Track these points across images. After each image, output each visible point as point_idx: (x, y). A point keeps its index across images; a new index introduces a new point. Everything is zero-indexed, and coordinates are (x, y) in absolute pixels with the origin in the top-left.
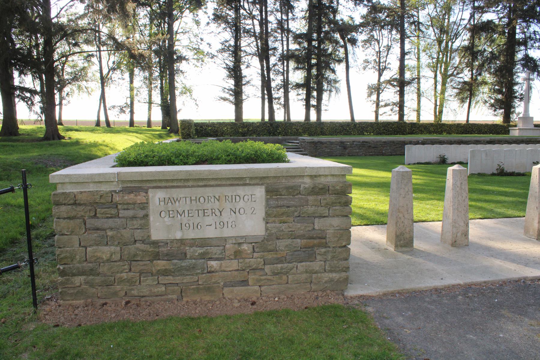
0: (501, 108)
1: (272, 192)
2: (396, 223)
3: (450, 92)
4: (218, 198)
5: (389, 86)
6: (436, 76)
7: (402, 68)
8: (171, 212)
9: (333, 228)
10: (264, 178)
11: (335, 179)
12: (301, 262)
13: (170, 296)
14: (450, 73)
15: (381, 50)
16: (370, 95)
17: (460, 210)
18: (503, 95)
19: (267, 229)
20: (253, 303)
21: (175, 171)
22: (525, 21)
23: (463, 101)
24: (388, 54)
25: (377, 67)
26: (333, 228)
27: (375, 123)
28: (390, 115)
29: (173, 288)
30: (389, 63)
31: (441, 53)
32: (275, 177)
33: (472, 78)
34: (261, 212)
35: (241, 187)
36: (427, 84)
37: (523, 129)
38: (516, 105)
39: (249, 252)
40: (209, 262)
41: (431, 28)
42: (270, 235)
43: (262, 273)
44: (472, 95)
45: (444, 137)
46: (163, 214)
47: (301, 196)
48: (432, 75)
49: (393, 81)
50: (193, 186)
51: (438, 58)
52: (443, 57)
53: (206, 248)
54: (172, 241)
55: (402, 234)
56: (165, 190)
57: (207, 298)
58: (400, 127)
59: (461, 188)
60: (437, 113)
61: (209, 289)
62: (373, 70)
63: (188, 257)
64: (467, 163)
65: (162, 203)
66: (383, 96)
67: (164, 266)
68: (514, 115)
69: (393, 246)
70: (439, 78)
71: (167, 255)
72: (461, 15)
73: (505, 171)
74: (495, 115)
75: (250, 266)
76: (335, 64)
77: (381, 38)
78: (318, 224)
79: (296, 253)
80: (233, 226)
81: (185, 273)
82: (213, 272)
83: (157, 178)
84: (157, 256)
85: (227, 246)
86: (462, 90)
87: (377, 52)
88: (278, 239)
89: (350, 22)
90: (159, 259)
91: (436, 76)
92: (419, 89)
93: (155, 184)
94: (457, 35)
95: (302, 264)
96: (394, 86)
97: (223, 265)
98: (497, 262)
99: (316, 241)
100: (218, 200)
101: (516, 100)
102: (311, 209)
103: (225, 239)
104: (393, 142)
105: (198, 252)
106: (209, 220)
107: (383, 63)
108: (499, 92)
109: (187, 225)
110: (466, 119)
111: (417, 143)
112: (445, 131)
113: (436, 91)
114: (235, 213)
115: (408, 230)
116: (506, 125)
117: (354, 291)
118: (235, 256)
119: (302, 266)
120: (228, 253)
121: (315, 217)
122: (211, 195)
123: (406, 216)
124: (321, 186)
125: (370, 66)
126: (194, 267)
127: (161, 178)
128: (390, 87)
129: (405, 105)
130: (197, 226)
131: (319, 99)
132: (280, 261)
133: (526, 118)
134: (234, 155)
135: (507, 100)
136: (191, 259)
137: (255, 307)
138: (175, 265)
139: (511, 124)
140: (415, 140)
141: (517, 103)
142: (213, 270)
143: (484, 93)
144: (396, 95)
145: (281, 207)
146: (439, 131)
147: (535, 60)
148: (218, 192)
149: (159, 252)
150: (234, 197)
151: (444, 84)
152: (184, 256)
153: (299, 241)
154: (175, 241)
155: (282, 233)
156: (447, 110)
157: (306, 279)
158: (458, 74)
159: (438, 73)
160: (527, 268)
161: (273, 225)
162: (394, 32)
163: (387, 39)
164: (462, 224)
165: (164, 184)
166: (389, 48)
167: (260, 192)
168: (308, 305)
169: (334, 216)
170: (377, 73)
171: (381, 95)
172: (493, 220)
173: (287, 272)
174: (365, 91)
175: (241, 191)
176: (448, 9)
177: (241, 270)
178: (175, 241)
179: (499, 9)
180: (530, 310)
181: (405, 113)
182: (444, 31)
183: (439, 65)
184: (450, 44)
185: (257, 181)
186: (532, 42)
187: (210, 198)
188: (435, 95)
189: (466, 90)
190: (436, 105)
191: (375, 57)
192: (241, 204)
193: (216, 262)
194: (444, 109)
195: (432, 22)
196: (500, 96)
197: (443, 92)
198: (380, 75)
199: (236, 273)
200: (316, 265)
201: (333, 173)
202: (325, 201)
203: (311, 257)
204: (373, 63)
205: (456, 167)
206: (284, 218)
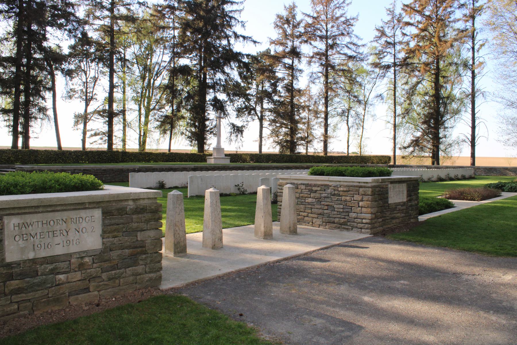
1: (106, 213)
2: (174, 235)
3: (153, 124)
4: (65, 220)
5: (96, 116)
6: (140, 109)
7: (110, 100)
8: (25, 236)
9: (150, 239)
10: (100, 202)
11: (150, 201)
12: (129, 267)
13: (21, 313)
14: (151, 107)
15: (88, 81)
16: (77, 123)
17: (216, 221)
19: (103, 243)
20: (98, 305)
21: (29, 200)
22: (212, 69)
23: (164, 132)
24: (94, 85)
25: (84, 97)
26: (150, 239)
29: (25, 304)
30: (95, 94)
32: (108, 201)
33: (172, 113)
34: (99, 230)
35: (84, 211)
37: (217, 158)
38: (208, 137)
39: (90, 263)
40: (57, 276)
41: (136, 65)
42: (105, 248)
43: (100, 280)
44: (172, 127)
45: (177, 164)
46: (17, 238)
47: (127, 216)
48: (137, 107)
50: (42, 212)
51: (142, 92)
53: (55, 264)
54: (25, 261)
55: (178, 243)
56: (20, 216)
57: (56, 308)
58: (110, 155)
59: (216, 205)
61: (57, 300)
62: (79, 99)
63: (39, 274)
64: (187, 187)
65: (17, 228)
66: (90, 125)
67: (17, 285)
69: (173, 253)
70: (143, 111)
71: (20, 274)
75: (91, 275)
76: (45, 92)
77: (88, 69)
78: (140, 236)
79: (125, 260)
80: (78, 243)
81: (37, 288)
82: (62, 284)
83: (12, 206)
84: (11, 277)
85: (73, 260)
86: (163, 123)
87: (84, 83)
88: (111, 250)
89: (58, 51)
90: (13, 280)
91: (140, 109)
92: (124, 120)
93: (8, 212)
94: (158, 74)
95: (129, 269)
96: (103, 116)
97: (69, 277)
98: (248, 256)
99: (139, 250)
100: (65, 222)
101: (208, 133)
102: (135, 225)
103: (70, 255)
104: (112, 170)
105: (49, 268)
106: (58, 240)
107: (89, 93)
109: (39, 246)
110: (168, 148)
111: (139, 170)
114: (79, 232)
115: (182, 239)
117: (166, 286)
118: (79, 268)
119: (130, 270)
120: (73, 267)
121: (138, 231)
122: (60, 218)
123: (181, 229)
124: (141, 207)
125: (77, 96)
126: (45, 282)
127: (16, 206)
128: (100, 117)
129: (114, 134)
130: (48, 246)
131: (26, 127)
132: (113, 268)
133: (218, 149)
134: (64, 184)
136: (42, 275)
137: (100, 307)
138: (28, 282)
140: (132, 168)
141: (209, 136)
142: (61, 282)
144: (105, 125)
145: (113, 225)
146: (145, 159)
148: (65, 215)
149: (12, 273)
150: (78, 219)
151: (147, 116)
152: (36, 274)
153: (127, 250)
154: (27, 262)
155: (114, 246)
157: (133, 280)
158: (160, 109)
159: (142, 106)
160: (267, 257)
161: (108, 240)
162: (101, 65)
163: (94, 71)
164: (218, 232)
165: (16, 211)
166: (95, 79)
167: (97, 214)
168: (139, 300)
169: (150, 230)
170: (83, 103)
171: (88, 124)
172: (229, 229)
173: (119, 277)
174: (72, 121)
175: (83, 213)
177: (83, 280)
178: (27, 262)
179: (191, 56)
180: (281, 278)
181: (114, 142)
184: (152, 81)
185: (95, 205)
186: (218, 87)
187: (58, 221)
188: (140, 125)
189: (167, 123)
190: (140, 135)
191: (82, 88)
192: (84, 224)
193: (64, 275)
194: (148, 139)
195: (137, 60)
196: (193, 130)
197: (146, 124)
198: (87, 105)
199: (80, 282)
200: (140, 269)
201: (149, 197)
202: (144, 218)
203: (135, 263)
204: (80, 92)
205: (174, 192)
206: (115, 234)
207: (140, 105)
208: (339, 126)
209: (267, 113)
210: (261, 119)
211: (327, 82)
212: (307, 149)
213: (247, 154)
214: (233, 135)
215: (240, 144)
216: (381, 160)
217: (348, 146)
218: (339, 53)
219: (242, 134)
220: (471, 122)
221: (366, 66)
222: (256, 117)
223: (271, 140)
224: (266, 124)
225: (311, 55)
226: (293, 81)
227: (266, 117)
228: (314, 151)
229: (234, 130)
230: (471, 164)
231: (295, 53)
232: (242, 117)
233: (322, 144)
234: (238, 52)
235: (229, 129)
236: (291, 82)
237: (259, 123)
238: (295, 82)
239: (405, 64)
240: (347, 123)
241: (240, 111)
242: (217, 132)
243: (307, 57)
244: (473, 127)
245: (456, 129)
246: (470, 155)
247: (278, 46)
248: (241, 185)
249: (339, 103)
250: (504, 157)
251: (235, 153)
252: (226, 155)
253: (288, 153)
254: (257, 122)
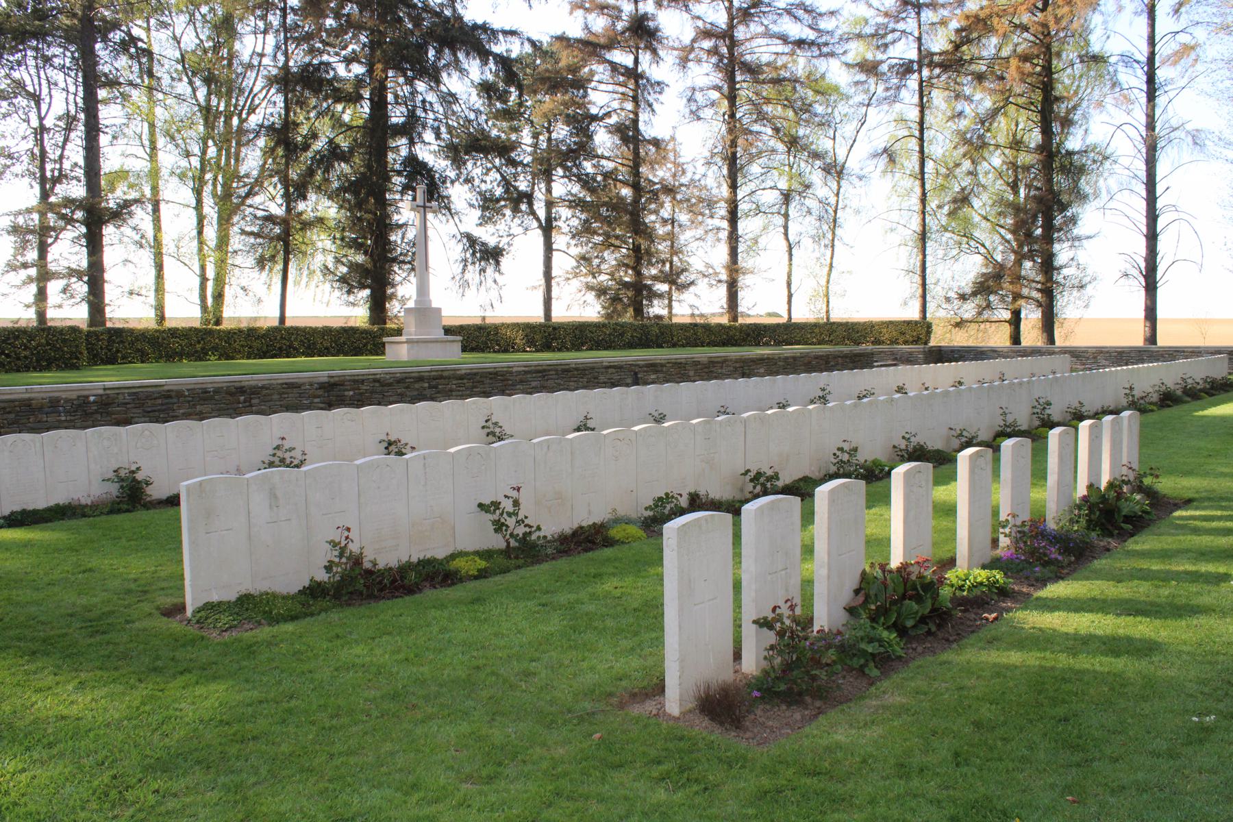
0: (362, 287)
6: (199, 202)
18: (366, 253)
27: (826, 324)
28: (60, 306)
31: (210, 143)
36: (178, 219)
37: (418, 341)
38: (398, 279)
48: (188, 196)
49: (65, 207)
52: (219, 155)
60: (210, 301)
62: (27, 180)
66: (54, 252)
68: (394, 302)
70: (210, 209)
72: (255, 43)
73: (367, 565)
74: (354, 304)
91: (199, 202)
108: (357, 245)
110: (277, 314)
112: (215, 349)
113: (201, 243)
116: (376, 328)
125: (18, 168)
133: (424, 312)
135: (375, 266)
139: (390, 325)
140: (74, 395)
143: (323, 249)
147: (431, 170)
151: (224, 221)
156: (232, 292)
176: (226, 28)
182: (215, 73)
183: (208, 176)
188: (200, 250)
190: (204, 280)
196: (360, 258)
204: (25, 159)
207: (198, 192)
208: (762, 242)
209: (564, 212)
210: (548, 228)
211: (732, 116)
212: (670, 307)
213: (516, 326)
214: (470, 267)
215: (494, 294)
216: (903, 334)
217: (790, 296)
218: (768, 34)
219: (498, 263)
220: (1144, 221)
221: (836, 73)
222: (535, 224)
223: (576, 283)
224: (560, 241)
225: (687, 40)
226: (636, 114)
227: (560, 223)
228: (689, 312)
229: (474, 254)
230: (1146, 340)
231: (642, 32)
232: (495, 223)
233: (723, 291)
234: (480, 22)
235: (457, 250)
236: (631, 116)
237: (541, 239)
238: (643, 117)
239: (952, 63)
240: (786, 234)
241: (489, 205)
242: (418, 261)
243: (673, 48)
244: (1152, 237)
245: (1101, 241)
246: (1141, 314)
247: (594, 15)
248: (508, 505)
249: (763, 184)
250: (1191, 317)
251: (479, 322)
252: (448, 331)
253: (628, 317)
254: (537, 236)
